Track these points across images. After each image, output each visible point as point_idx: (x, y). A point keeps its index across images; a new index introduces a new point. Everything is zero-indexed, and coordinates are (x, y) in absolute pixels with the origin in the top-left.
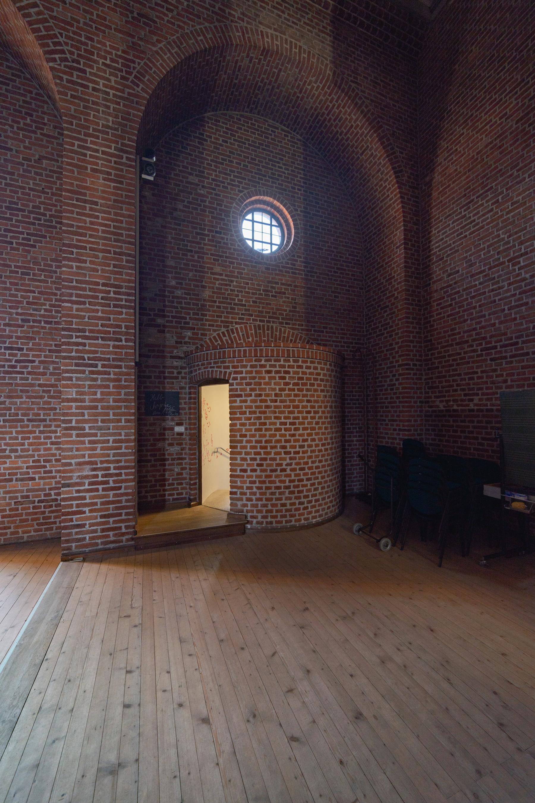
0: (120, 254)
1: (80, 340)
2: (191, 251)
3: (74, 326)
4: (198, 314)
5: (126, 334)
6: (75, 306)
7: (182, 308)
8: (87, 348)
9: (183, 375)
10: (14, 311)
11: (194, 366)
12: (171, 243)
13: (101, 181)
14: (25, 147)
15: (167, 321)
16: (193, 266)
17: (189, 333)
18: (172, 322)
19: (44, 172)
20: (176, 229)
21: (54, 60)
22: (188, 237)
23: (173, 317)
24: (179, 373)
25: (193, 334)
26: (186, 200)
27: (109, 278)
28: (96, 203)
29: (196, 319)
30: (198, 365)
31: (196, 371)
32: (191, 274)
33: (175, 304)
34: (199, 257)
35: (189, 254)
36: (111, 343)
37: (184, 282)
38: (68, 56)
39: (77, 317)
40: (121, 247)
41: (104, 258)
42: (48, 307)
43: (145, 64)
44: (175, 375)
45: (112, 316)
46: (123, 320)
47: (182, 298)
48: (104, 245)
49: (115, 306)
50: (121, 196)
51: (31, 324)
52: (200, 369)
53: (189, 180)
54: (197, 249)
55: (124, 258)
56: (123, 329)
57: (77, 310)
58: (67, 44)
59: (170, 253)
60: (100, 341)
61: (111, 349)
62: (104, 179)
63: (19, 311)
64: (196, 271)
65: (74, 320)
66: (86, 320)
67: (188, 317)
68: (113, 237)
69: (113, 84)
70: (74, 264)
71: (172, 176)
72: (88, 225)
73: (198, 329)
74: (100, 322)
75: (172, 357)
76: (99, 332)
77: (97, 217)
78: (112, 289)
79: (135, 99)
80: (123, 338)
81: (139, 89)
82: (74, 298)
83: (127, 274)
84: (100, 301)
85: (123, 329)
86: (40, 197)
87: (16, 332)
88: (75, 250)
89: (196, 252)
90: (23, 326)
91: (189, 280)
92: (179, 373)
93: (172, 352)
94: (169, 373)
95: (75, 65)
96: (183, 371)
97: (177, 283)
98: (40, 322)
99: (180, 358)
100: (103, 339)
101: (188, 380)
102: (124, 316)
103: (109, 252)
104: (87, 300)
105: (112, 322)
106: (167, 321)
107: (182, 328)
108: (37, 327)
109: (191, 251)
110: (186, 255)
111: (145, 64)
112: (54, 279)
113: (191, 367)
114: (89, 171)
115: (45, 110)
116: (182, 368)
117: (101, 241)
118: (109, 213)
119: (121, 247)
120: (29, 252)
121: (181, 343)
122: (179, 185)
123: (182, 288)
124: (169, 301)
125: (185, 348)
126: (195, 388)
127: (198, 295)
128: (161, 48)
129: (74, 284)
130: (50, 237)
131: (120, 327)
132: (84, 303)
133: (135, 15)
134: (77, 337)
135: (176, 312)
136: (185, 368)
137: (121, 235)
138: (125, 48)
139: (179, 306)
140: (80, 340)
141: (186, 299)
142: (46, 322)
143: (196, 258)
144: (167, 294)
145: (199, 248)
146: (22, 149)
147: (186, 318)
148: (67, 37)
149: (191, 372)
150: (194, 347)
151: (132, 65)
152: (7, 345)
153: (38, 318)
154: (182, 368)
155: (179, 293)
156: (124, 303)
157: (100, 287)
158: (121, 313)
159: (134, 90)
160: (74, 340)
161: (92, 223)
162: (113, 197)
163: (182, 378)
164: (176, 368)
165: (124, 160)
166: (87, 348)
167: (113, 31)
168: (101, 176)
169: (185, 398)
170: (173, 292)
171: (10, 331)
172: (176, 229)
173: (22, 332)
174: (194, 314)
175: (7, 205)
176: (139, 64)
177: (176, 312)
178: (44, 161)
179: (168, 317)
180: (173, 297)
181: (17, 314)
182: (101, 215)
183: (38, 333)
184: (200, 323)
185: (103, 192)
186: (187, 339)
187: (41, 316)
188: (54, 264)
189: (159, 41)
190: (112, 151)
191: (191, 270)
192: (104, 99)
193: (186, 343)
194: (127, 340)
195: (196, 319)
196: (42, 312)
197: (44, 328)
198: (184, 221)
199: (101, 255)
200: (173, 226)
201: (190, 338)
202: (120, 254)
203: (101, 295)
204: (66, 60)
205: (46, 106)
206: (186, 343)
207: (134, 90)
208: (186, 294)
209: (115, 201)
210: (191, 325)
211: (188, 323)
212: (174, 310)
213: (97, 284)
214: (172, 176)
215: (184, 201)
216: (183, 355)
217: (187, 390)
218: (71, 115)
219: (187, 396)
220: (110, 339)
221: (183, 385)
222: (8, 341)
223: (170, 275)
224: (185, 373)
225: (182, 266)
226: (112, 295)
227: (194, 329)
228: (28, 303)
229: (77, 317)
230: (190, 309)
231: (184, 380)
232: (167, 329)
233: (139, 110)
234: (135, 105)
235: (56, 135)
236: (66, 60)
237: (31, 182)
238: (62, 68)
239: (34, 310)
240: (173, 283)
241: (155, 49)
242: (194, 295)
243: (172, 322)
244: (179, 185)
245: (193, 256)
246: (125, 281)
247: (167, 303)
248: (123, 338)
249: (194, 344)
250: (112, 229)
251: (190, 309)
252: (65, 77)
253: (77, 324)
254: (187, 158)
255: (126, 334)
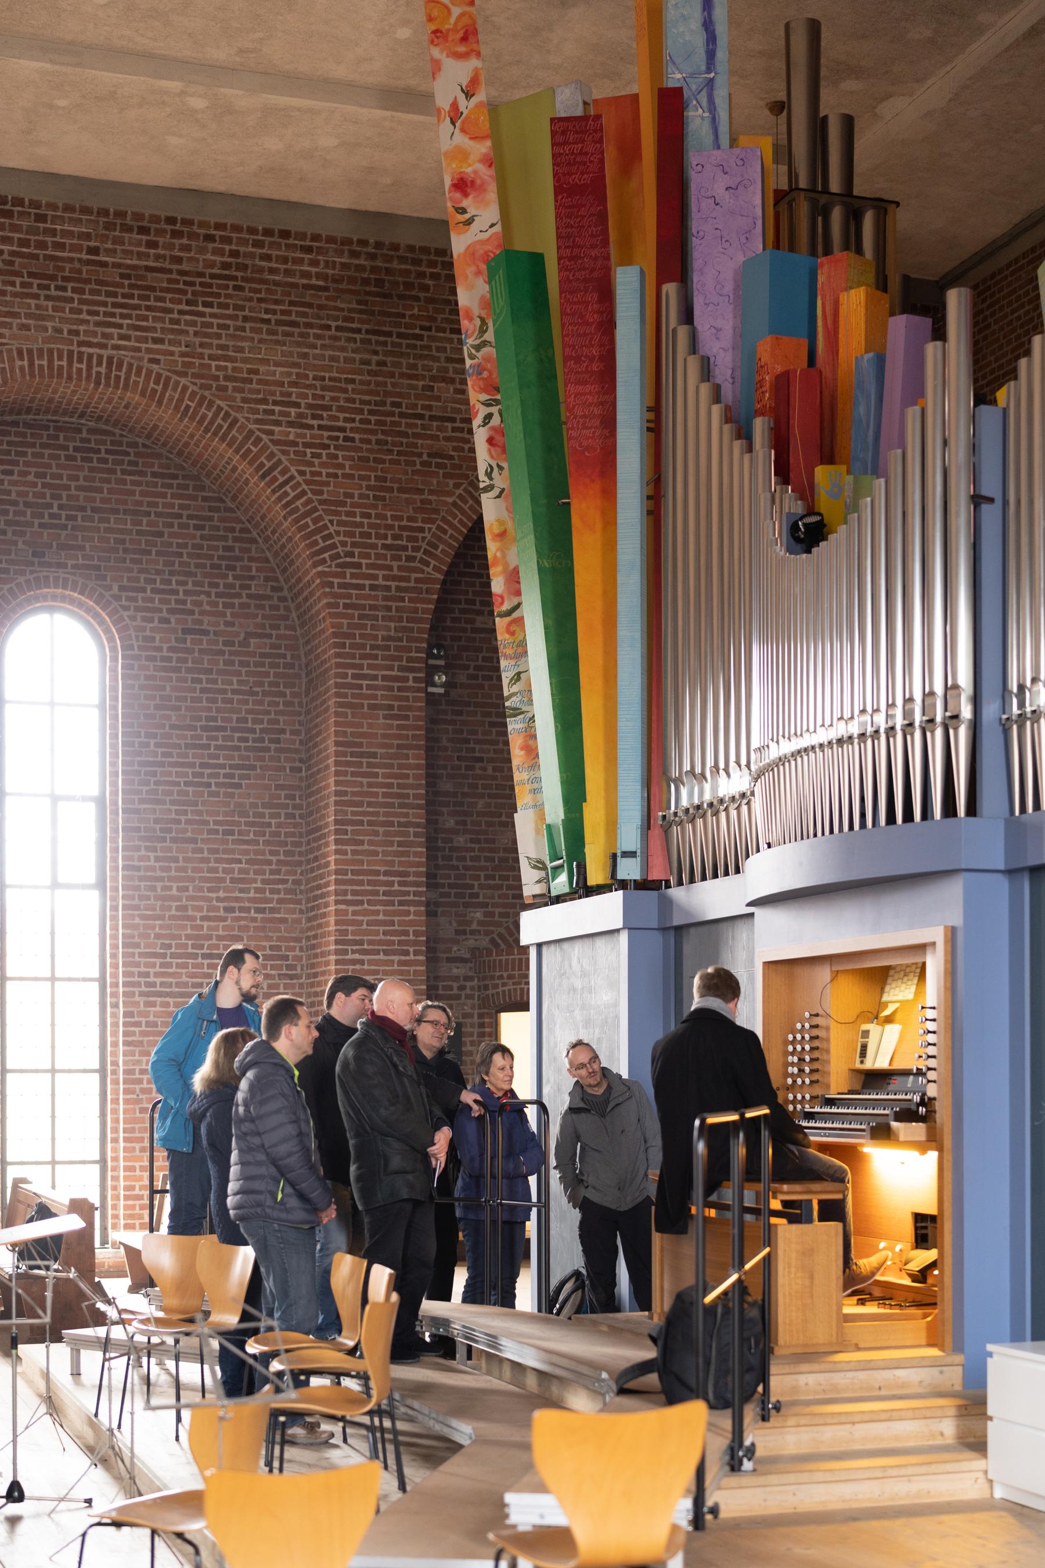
0: (407, 825)
1: (357, 956)
2: (481, 759)
3: (350, 937)
4: (493, 878)
5: (415, 943)
6: (351, 909)
7: (466, 868)
8: (366, 967)
9: (468, 991)
10: (214, 895)
11: (493, 978)
12: (445, 749)
13: (382, 721)
14: (227, 624)
15: (442, 895)
16: (485, 787)
17: (478, 915)
18: (448, 895)
19: (252, 660)
20: (454, 722)
21: (323, 562)
22: (475, 733)
23: (450, 886)
24: (462, 988)
25: (486, 914)
26: (472, 664)
27: (392, 863)
28: (374, 755)
29: (490, 887)
30: (501, 977)
31: (496, 986)
32: (481, 803)
33: (454, 863)
34: (494, 769)
35: (478, 765)
36: (396, 958)
37: (469, 819)
38: (340, 549)
39: (353, 923)
40: (407, 815)
41: (386, 834)
42: (259, 885)
43: (439, 528)
44: (455, 991)
45: (396, 919)
46: (411, 923)
47: (467, 850)
48: (386, 814)
49: (401, 903)
50: (407, 737)
51: (237, 914)
52: (504, 985)
53: (478, 625)
54: (492, 755)
55: (411, 830)
56: (411, 937)
57: (354, 913)
58: (338, 533)
59: (445, 767)
60: (381, 957)
61: (396, 967)
62: (385, 717)
63: (221, 894)
64: (490, 796)
65: (350, 928)
66: (365, 927)
67: (476, 883)
68: (397, 801)
69: (396, 572)
70: (349, 848)
71: (448, 623)
72: (365, 789)
73: (494, 905)
74: (381, 929)
75: (450, 960)
76: (380, 942)
77: (376, 775)
78: (396, 879)
79: (425, 586)
80: (411, 950)
81: (430, 570)
82: (349, 897)
83: (416, 854)
84: (382, 898)
85: (411, 937)
86: (246, 702)
87: (217, 929)
88: (349, 828)
89: (491, 760)
90: (225, 919)
91: (479, 814)
92: (462, 988)
93: (449, 950)
94: (445, 988)
95: (348, 559)
96: (468, 984)
97: (457, 823)
98: (248, 910)
99: (464, 961)
100: (386, 953)
101: (476, 1002)
102: (412, 917)
103: (391, 824)
104: (365, 898)
105: (396, 927)
106: (442, 895)
107: (466, 905)
108: (243, 918)
109: (481, 759)
110: (472, 768)
111: (439, 528)
112: (267, 837)
113: (484, 978)
114: (366, 709)
115: (253, 554)
116: (467, 978)
117: (382, 810)
118: (391, 766)
119: (407, 815)
120: (232, 795)
121: (464, 932)
122: (460, 639)
123: (466, 832)
124: (444, 858)
125: (471, 943)
126: (490, 1015)
127: (493, 841)
128: (460, 496)
129: (350, 876)
130: (261, 767)
131: (406, 933)
132: (361, 903)
133: (425, 457)
134: (354, 952)
135: (457, 877)
136: (471, 979)
137: (407, 796)
138: (411, 513)
139: (461, 864)
140: (357, 956)
141: (473, 850)
142: (258, 910)
143: (490, 771)
144: (440, 844)
145: (495, 752)
146: (222, 627)
147: (472, 887)
148: (340, 523)
149: (486, 988)
150: (488, 939)
151: (421, 535)
152: (205, 951)
153: (247, 904)
154: (467, 978)
155: (460, 840)
156: (411, 898)
157: (381, 878)
158: (408, 913)
159: (423, 572)
160: (350, 957)
161: (370, 785)
162: (395, 742)
163: (468, 997)
164: (456, 978)
165: (411, 683)
166: (366, 967)
167: (396, 493)
168: (381, 713)
169: (472, 1035)
170: (451, 841)
171: (209, 928)
172: (454, 722)
173: (225, 928)
174: (487, 877)
175: (204, 723)
176: (430, 529)
177: (457, 877)
178: (252, 641)
179: (443, 886)
180: (451, 849)
181: (218, 899)
182: (380, 771)
183: (246, 928)
184: (497, 893)
185: (384, 736)
186: (474, 926)
187: (250, 900)
188: (267, 811)
189: (457, 486)
190: (395, 673)
191: (482, 796)
192: (386, 598)
193: (473, 932)
194: (416, 953)
195: (490, 887)
196: (252, 894)
197: (255, 920)
198: (468, 704)
199: (381, 830)
200: (449, 718)
201: (481, 923)
202: (407, 825)
203: (382, 889)
204: (337, 556)
205: (254, 547)
206: (473, 932)
207: (423, 572)
208: (472, 841)
209: (399, 746)
210: (481, 900)
211: (477, 895)
212: (452, 873)
213: (377, 873)
214: (448, 623)
215: (467, 667)
216: (468, 956)
217: (476, 1019)
218: (345, 633)
219: (476, 1030)
220: (394, 953)
221: (467, 1009)
222: (206, 943)
223: (445, 809)
224: (472, 988)
225: (466, 790)
226: (396, 887)
227: (486, 905)
228: (232, 880)
229: (353, 923)
230: (481, 869)
231: (470, 1002)
232: (440, 910)
233: (429, 602)
234: (424, 595)
235: (268, 592)
236: (337, 556)
237: (235, 679)
238: (334, 569)
239: (241, 891)
240: (450, 823)
241: (450, 500)
242: (487, 841)
243: (448, 895)
244: (460, 639)
245: (484, 769)
246: (412, 864)
247: (440, 862)
248: (411, 950)
249: (487, 933)
250: (395, 790)
251: (481, 869)
252: (336, 581)
253: (354, 933)
254: (473, 584)
255: (415, 943)
